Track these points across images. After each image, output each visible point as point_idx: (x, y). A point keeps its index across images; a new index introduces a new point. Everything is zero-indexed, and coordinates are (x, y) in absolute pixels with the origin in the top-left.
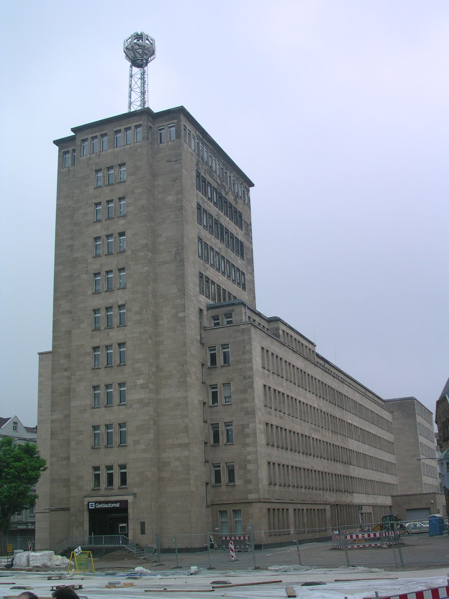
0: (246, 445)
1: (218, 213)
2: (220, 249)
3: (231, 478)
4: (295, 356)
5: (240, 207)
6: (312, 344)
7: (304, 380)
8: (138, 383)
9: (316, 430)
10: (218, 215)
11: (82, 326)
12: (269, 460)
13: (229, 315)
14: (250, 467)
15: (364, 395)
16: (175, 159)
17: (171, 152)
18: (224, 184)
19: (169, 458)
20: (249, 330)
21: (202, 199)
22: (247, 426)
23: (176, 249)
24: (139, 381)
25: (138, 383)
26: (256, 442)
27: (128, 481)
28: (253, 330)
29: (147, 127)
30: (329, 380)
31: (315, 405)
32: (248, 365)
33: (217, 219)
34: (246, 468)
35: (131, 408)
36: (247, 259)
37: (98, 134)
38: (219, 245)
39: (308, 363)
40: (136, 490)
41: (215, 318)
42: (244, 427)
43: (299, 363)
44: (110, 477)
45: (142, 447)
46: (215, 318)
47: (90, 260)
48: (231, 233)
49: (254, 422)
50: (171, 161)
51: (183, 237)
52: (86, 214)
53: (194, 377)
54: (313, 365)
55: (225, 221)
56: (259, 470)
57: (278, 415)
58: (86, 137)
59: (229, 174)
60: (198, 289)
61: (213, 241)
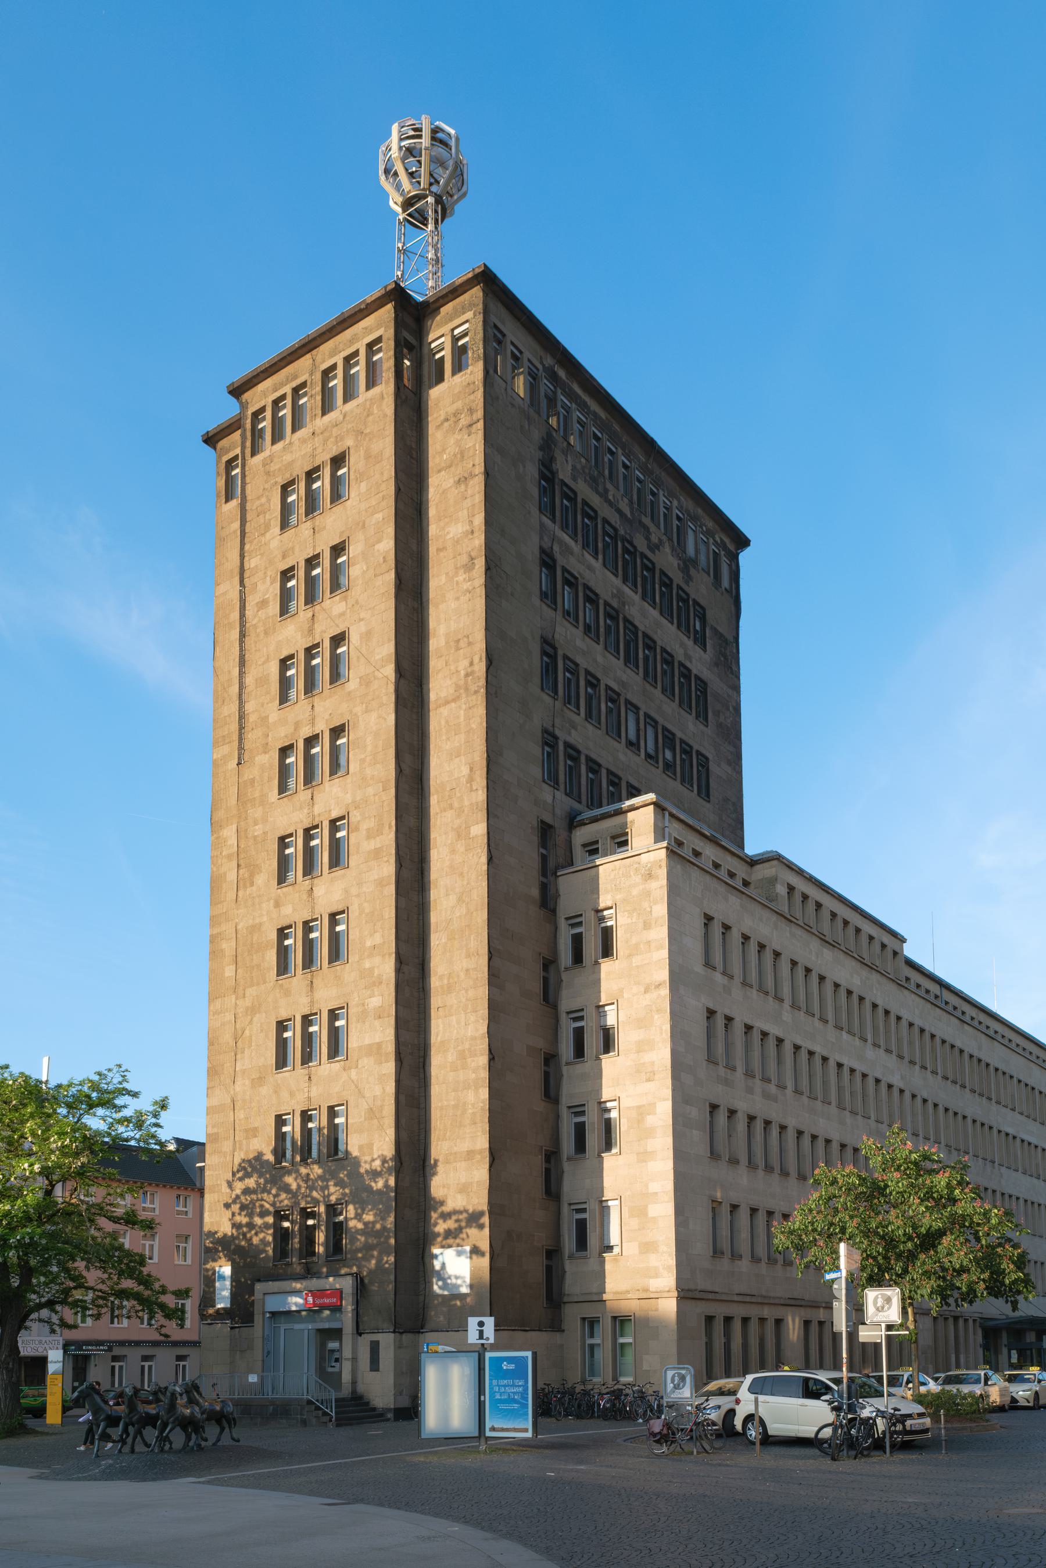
2: (623, 684)
4: (828, 954)
5: (700, 589)
6: (894, 934)
7: (854, 1011)
8: (371, 1006)
15: (935, 1002)
18: (647, 521)
23: (466, 663)
25: (371, 1006)
30: (945, 1027)
31: (897, 1081)
33: (615, 604)
34: (645, 1214)
36: (720, 725)
39: (875, 976)
43: (845, 972)
48: (663, 650)
54: (893, 987)
58: (262, 404)
59: (662, 498)
60: (536, 771)
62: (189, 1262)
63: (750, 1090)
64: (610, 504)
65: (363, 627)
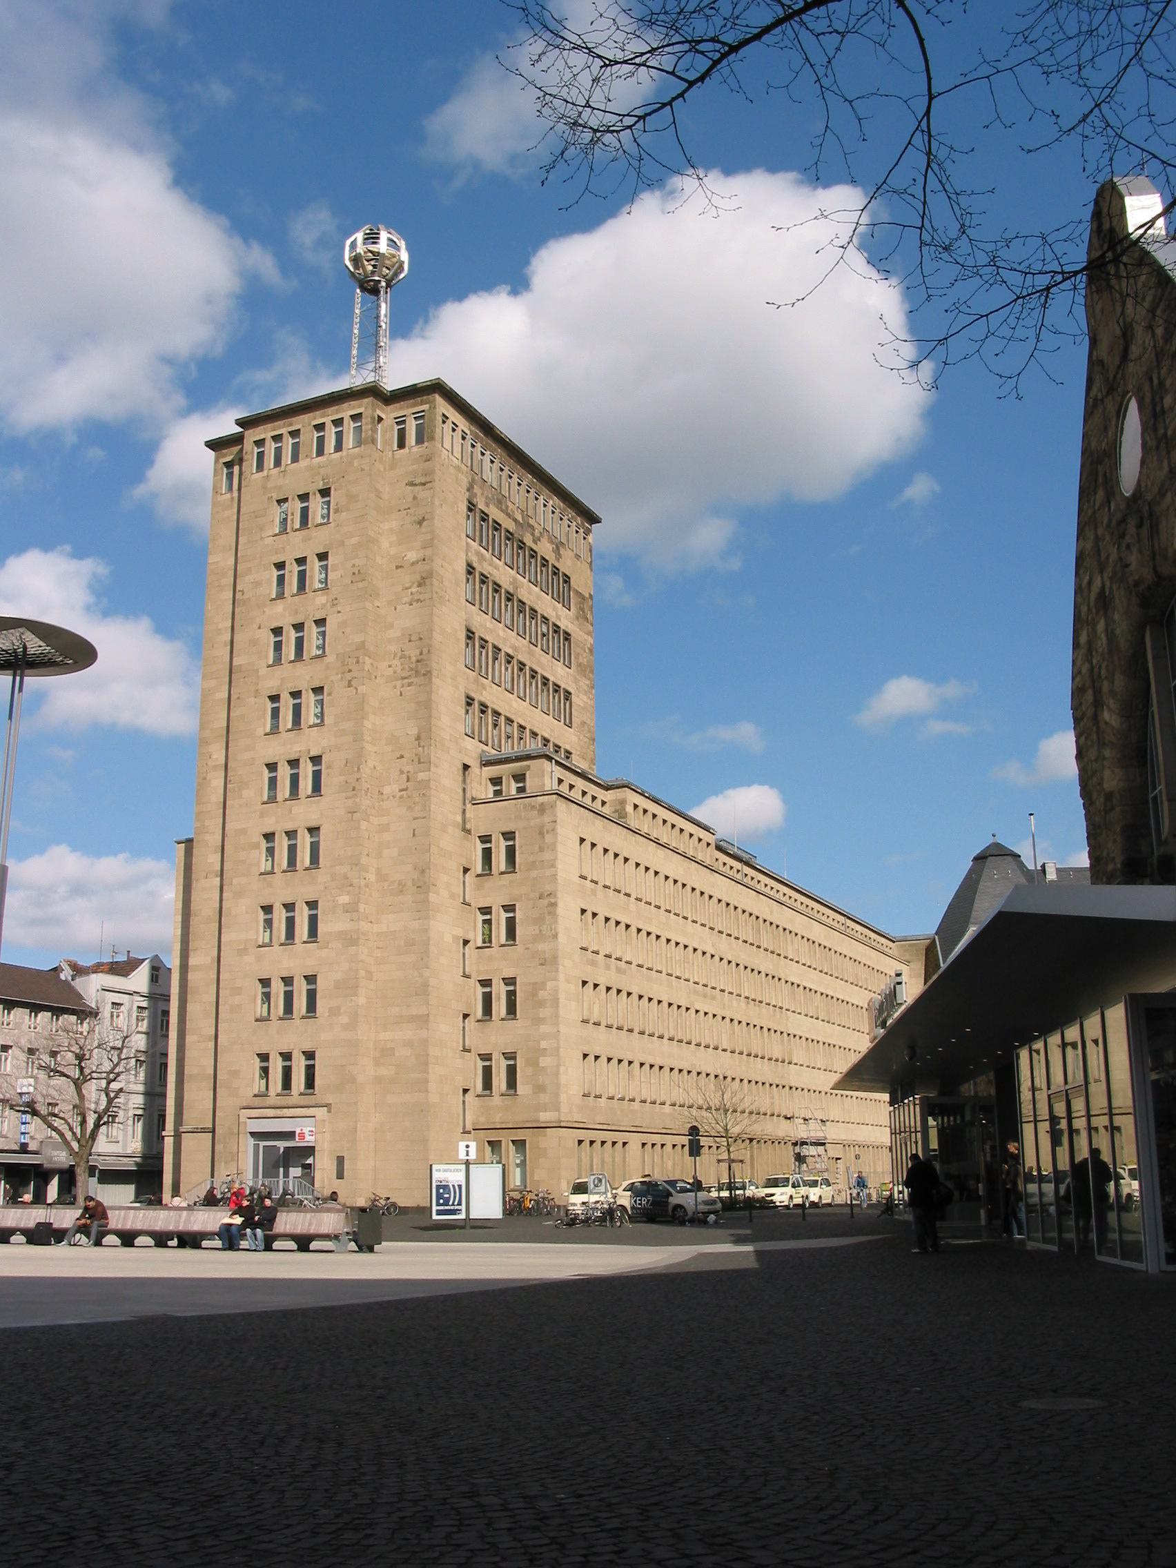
0: (538, 1021)
1: (515, 579)
2: (516, 649)
3: (512, 1083)
9: (705, 996)
10: (514, 581)
12: (586, 1050)
13: (520, 777)
14: (545, 1062)
18: (531, 522)
20: (553, 806)
21: (478, 553)
22: (542, 985)
23: (418, 652)
26: (557, 1016)
27: (318, 1081)
28: (561, 805)
29: (373, 418)
32: (548, 872)
33: (511, 591)
36: (579, 665)
37: (284, 431)
38: (513, 640)
40: (330, 1099)
41: (496, 781)
42: (536, 987)
46: (496, 781)
47: (263, 671)
49: (556, 979)
51: (431, 631)
53: (444, 893)
55: (530, 593)
56: (562, 1069)
57: (613, 968)
58: (262, 437)
61: (501, 633)
62: (435, 1217)
63: (608, 968)
64: (508, 515)
65: (340, 617)
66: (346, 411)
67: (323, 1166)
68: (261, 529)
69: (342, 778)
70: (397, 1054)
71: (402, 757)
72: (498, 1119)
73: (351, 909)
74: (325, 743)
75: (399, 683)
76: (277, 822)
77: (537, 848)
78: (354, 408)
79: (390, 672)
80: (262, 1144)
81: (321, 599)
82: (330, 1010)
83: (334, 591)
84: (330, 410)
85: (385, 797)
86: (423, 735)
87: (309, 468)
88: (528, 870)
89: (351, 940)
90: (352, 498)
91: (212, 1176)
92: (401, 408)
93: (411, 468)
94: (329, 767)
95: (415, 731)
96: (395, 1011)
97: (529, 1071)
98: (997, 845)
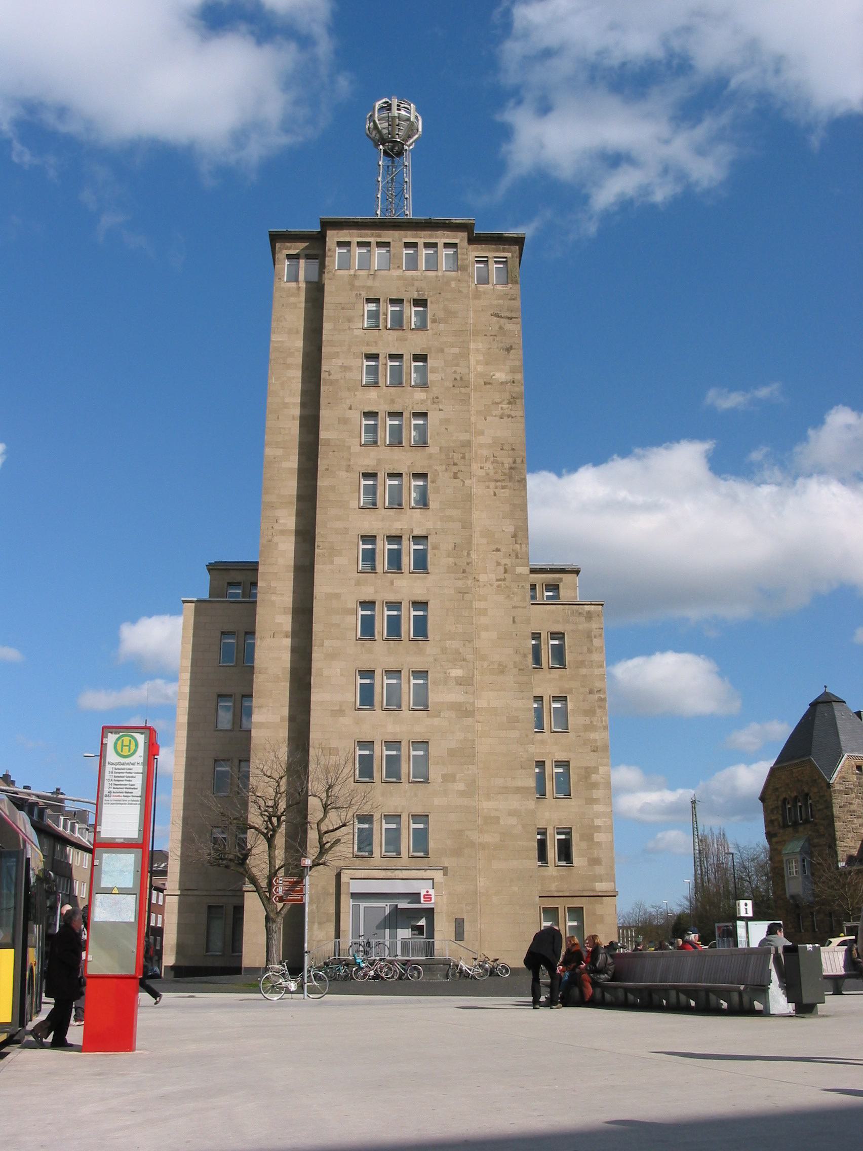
0: (591, 801)
11: (338, 560)
13: (554, 587)
14: (599, 837)
16: (508, 314)
17: (501, 302)
19: (496, 810)
22: (595, 770)
23: (511, 460)
24: (454, 671)
34: (593, 839)
35: (439, 716)
37: (373, 240)
42: (588, 771)
44: (393, 839)
45: (461, 786)
50: (501, 317)
52: (346, 368)
66: (441, 238)
67: (443, 929)
68: (350, 320)
69: (451, 560)
70: (502, 822)
71: (498, 550)
72: (553, 888)
73: (465, 682)
74: (430, 525)
75: (492, 485)
76: (376, 592)
77: (585, 649)
78: (448, 237)
79: (482, 473)
80: (363, 905)
81: (420, 395)
82: (444, 776)
83: (435, 390)
84: (423, 233)
85: (481, 584)
86: (520, 534)
87: (400, 278)
88: (578, 667)
89: (464, 711)
90: (450, 314)
91: (338, 936)
92: (482, 250)
93: (495, 302)
94: (435, 548)
95: (511, 529)
96: (500, 782)
97: (584, 845)
98: (825, 694)
